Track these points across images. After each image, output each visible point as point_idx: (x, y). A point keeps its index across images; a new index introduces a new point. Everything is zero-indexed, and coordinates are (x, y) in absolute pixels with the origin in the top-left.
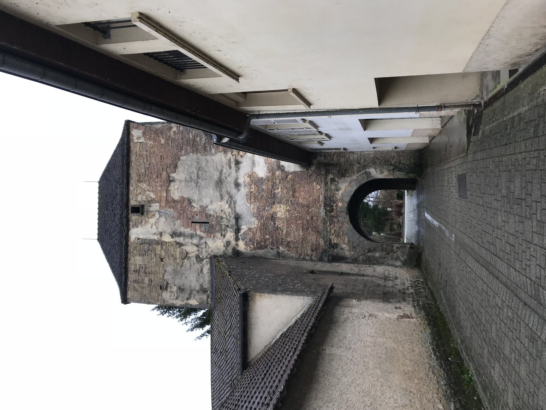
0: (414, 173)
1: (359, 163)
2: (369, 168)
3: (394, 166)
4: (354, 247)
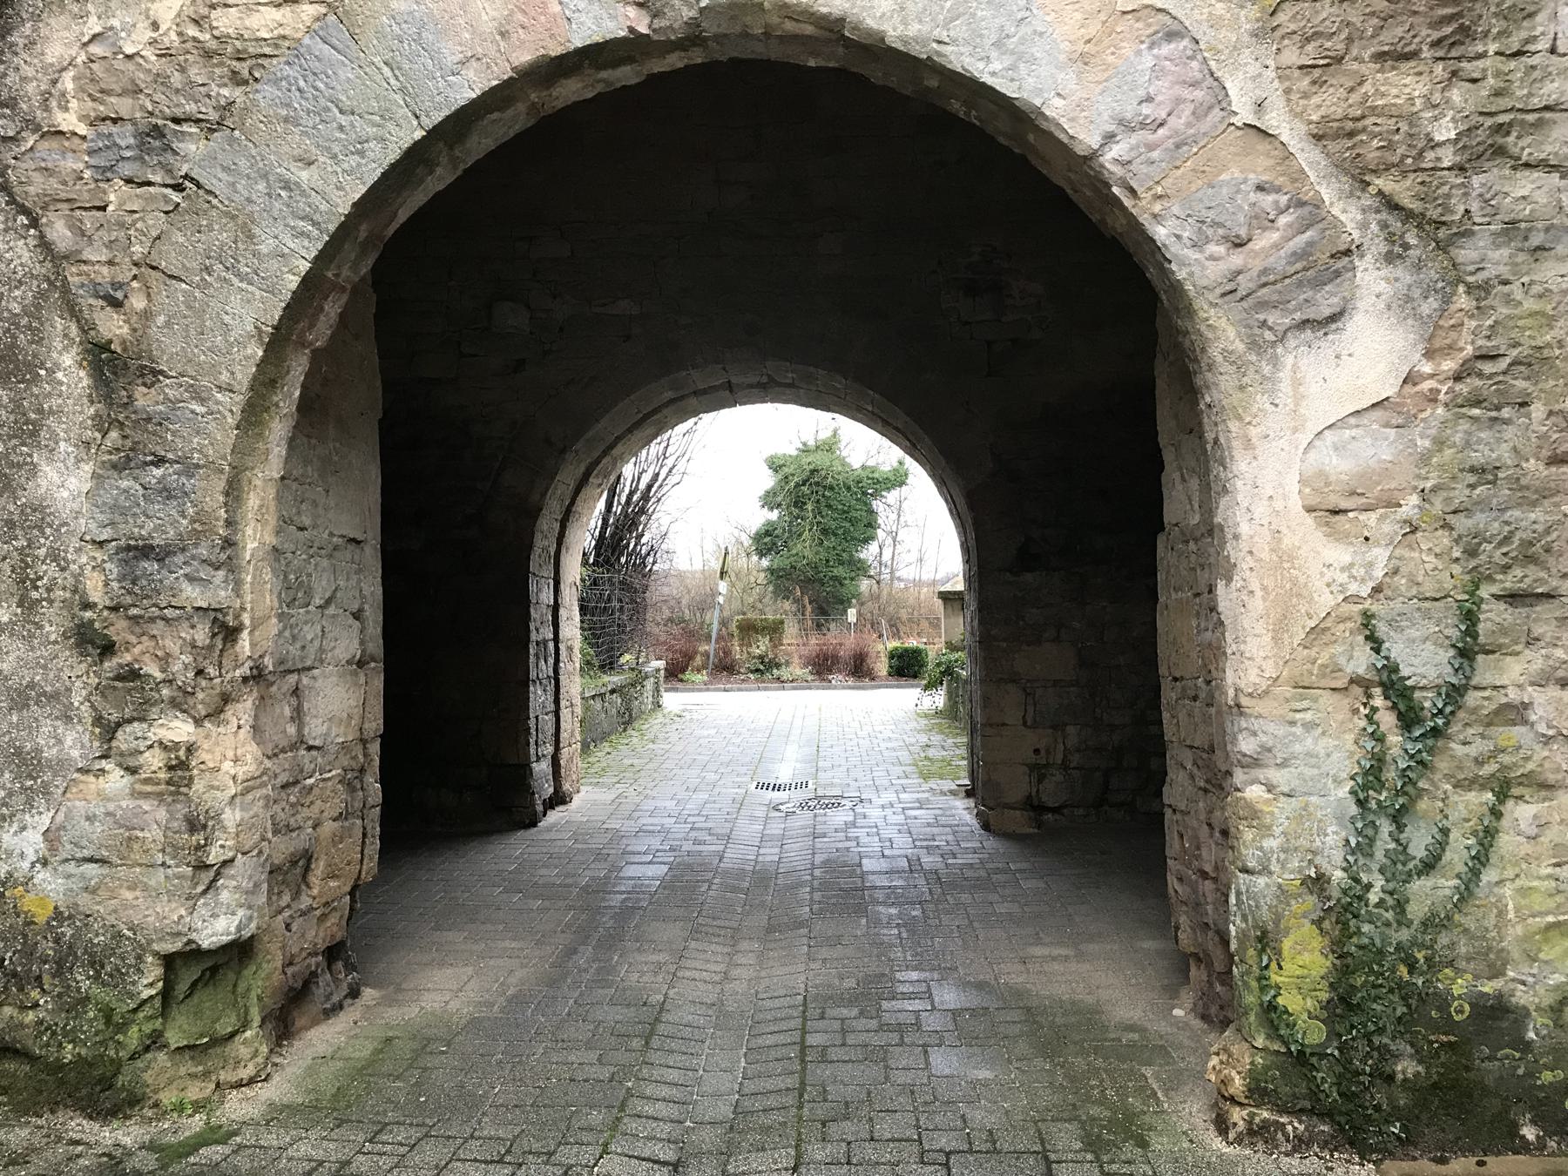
0: (1342, 1004)
1: (1489, 145)
2: (1404, 303)
3: (1455, 693)
4: (154, 137)
